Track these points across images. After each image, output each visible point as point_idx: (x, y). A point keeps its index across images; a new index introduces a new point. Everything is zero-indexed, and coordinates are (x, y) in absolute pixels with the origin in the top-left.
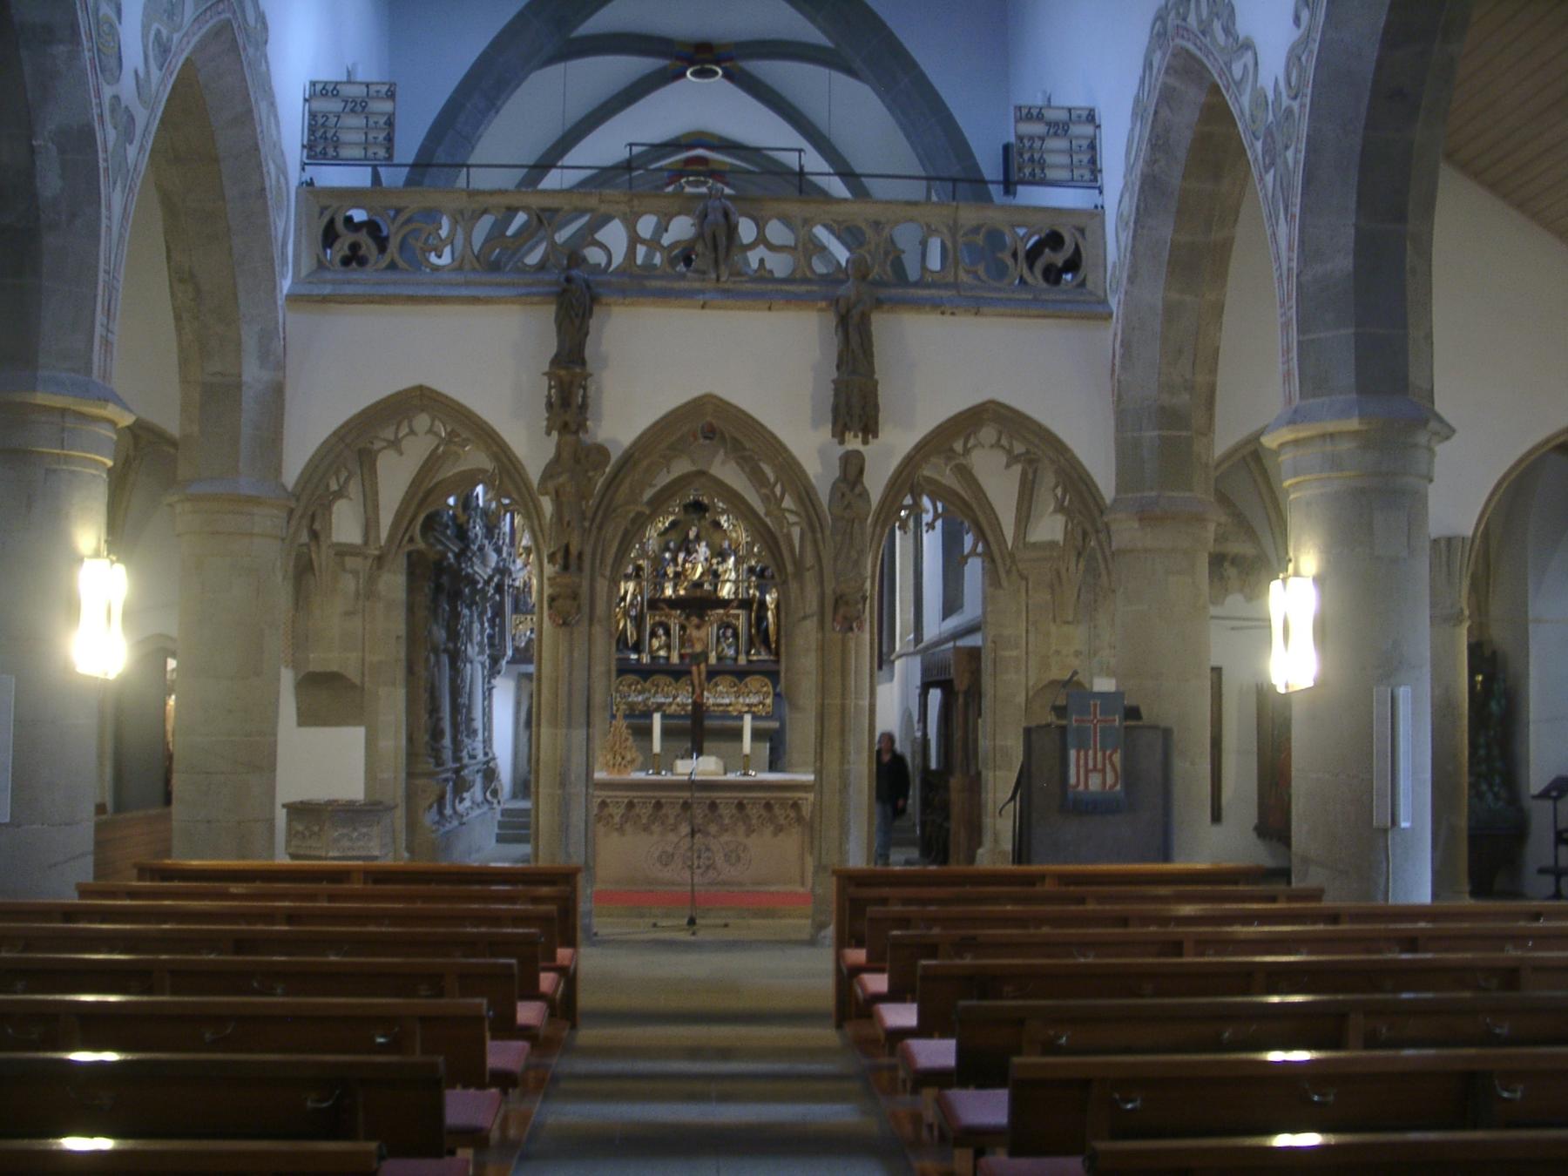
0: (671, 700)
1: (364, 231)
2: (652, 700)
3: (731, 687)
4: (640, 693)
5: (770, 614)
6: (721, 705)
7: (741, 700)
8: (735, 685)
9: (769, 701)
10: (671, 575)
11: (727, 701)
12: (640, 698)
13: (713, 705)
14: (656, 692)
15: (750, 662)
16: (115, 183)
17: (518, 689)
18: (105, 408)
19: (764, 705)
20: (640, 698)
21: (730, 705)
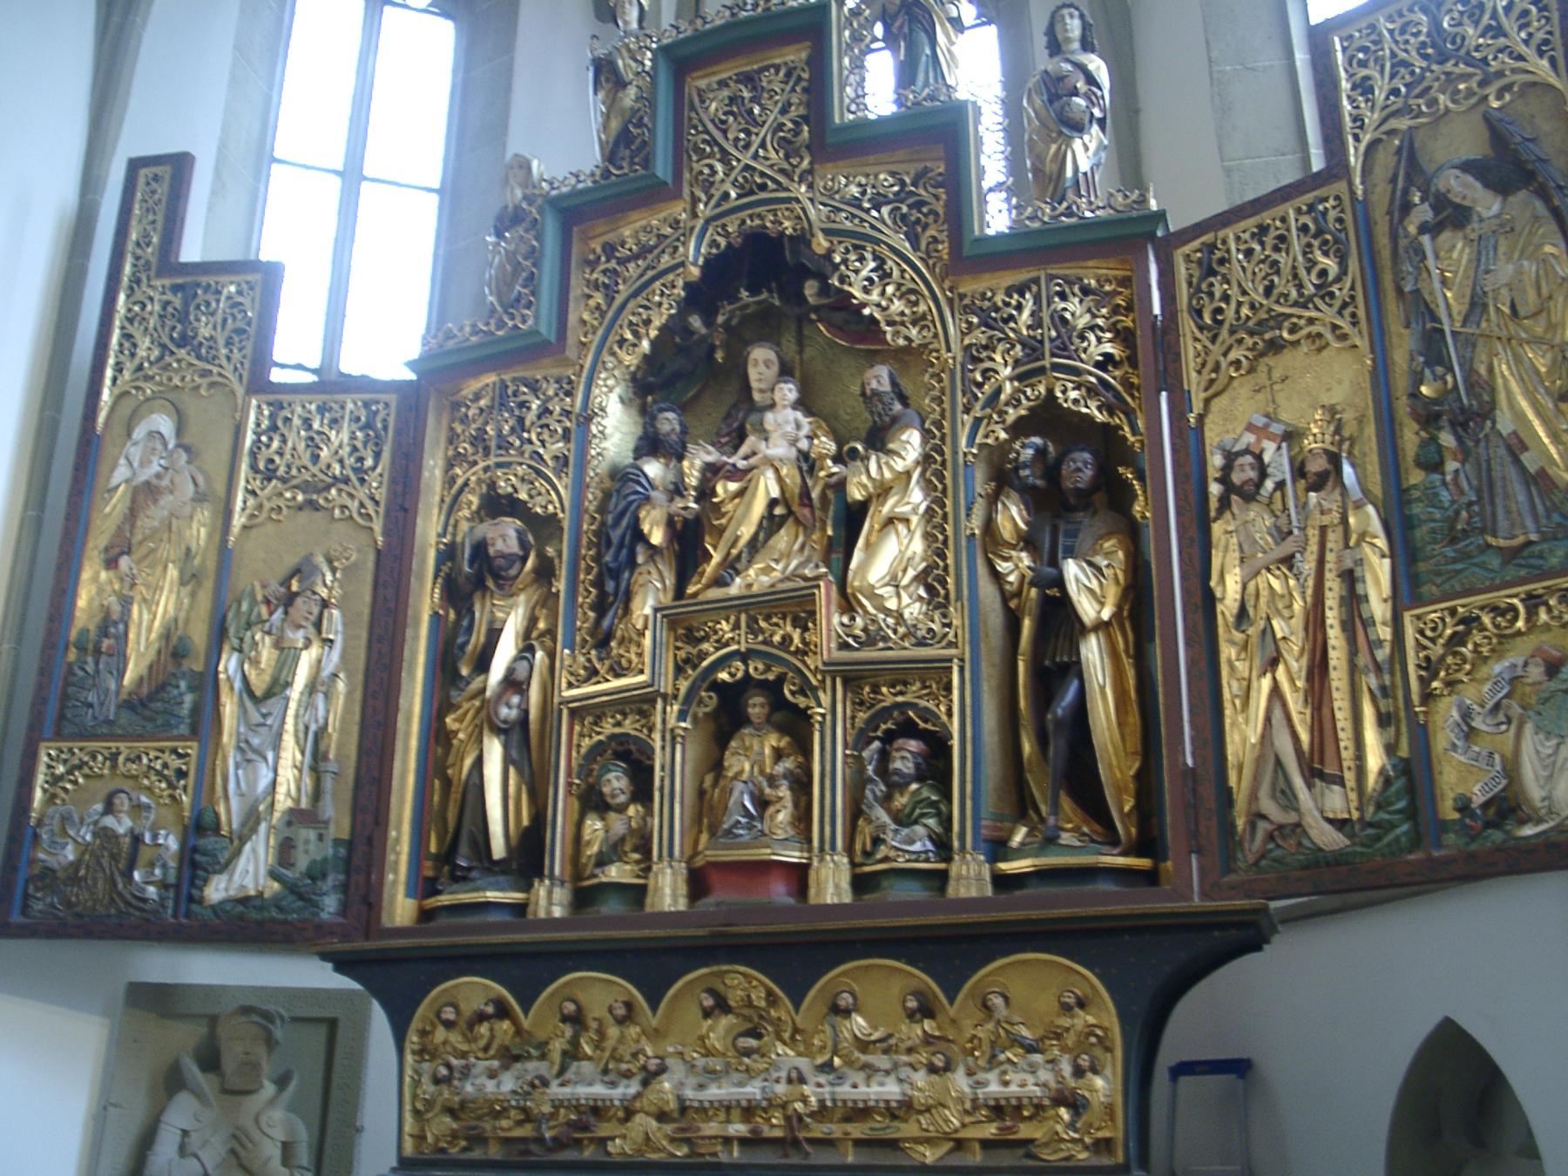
0: (633, 1088)
1: (816, 167)
2: (555, 1090)
3: (911, 1015)
4: (510, 1058)
5: (1092, 651)
6: (860, 1112)
7: (960, 1081)
8: (926, 1010)
9: (1102, 1086)
10: (657, 537)
11: (891, 1090)
12: (508, 1083)
13: (822, 1112)
14: (572, 1054)
15: (1002, 882)
16: (969, 509)
17: (121, 1049)
18: (408, 895)
19: (1077, 1105)
20: (508, 1083)
21: (904, 1109)
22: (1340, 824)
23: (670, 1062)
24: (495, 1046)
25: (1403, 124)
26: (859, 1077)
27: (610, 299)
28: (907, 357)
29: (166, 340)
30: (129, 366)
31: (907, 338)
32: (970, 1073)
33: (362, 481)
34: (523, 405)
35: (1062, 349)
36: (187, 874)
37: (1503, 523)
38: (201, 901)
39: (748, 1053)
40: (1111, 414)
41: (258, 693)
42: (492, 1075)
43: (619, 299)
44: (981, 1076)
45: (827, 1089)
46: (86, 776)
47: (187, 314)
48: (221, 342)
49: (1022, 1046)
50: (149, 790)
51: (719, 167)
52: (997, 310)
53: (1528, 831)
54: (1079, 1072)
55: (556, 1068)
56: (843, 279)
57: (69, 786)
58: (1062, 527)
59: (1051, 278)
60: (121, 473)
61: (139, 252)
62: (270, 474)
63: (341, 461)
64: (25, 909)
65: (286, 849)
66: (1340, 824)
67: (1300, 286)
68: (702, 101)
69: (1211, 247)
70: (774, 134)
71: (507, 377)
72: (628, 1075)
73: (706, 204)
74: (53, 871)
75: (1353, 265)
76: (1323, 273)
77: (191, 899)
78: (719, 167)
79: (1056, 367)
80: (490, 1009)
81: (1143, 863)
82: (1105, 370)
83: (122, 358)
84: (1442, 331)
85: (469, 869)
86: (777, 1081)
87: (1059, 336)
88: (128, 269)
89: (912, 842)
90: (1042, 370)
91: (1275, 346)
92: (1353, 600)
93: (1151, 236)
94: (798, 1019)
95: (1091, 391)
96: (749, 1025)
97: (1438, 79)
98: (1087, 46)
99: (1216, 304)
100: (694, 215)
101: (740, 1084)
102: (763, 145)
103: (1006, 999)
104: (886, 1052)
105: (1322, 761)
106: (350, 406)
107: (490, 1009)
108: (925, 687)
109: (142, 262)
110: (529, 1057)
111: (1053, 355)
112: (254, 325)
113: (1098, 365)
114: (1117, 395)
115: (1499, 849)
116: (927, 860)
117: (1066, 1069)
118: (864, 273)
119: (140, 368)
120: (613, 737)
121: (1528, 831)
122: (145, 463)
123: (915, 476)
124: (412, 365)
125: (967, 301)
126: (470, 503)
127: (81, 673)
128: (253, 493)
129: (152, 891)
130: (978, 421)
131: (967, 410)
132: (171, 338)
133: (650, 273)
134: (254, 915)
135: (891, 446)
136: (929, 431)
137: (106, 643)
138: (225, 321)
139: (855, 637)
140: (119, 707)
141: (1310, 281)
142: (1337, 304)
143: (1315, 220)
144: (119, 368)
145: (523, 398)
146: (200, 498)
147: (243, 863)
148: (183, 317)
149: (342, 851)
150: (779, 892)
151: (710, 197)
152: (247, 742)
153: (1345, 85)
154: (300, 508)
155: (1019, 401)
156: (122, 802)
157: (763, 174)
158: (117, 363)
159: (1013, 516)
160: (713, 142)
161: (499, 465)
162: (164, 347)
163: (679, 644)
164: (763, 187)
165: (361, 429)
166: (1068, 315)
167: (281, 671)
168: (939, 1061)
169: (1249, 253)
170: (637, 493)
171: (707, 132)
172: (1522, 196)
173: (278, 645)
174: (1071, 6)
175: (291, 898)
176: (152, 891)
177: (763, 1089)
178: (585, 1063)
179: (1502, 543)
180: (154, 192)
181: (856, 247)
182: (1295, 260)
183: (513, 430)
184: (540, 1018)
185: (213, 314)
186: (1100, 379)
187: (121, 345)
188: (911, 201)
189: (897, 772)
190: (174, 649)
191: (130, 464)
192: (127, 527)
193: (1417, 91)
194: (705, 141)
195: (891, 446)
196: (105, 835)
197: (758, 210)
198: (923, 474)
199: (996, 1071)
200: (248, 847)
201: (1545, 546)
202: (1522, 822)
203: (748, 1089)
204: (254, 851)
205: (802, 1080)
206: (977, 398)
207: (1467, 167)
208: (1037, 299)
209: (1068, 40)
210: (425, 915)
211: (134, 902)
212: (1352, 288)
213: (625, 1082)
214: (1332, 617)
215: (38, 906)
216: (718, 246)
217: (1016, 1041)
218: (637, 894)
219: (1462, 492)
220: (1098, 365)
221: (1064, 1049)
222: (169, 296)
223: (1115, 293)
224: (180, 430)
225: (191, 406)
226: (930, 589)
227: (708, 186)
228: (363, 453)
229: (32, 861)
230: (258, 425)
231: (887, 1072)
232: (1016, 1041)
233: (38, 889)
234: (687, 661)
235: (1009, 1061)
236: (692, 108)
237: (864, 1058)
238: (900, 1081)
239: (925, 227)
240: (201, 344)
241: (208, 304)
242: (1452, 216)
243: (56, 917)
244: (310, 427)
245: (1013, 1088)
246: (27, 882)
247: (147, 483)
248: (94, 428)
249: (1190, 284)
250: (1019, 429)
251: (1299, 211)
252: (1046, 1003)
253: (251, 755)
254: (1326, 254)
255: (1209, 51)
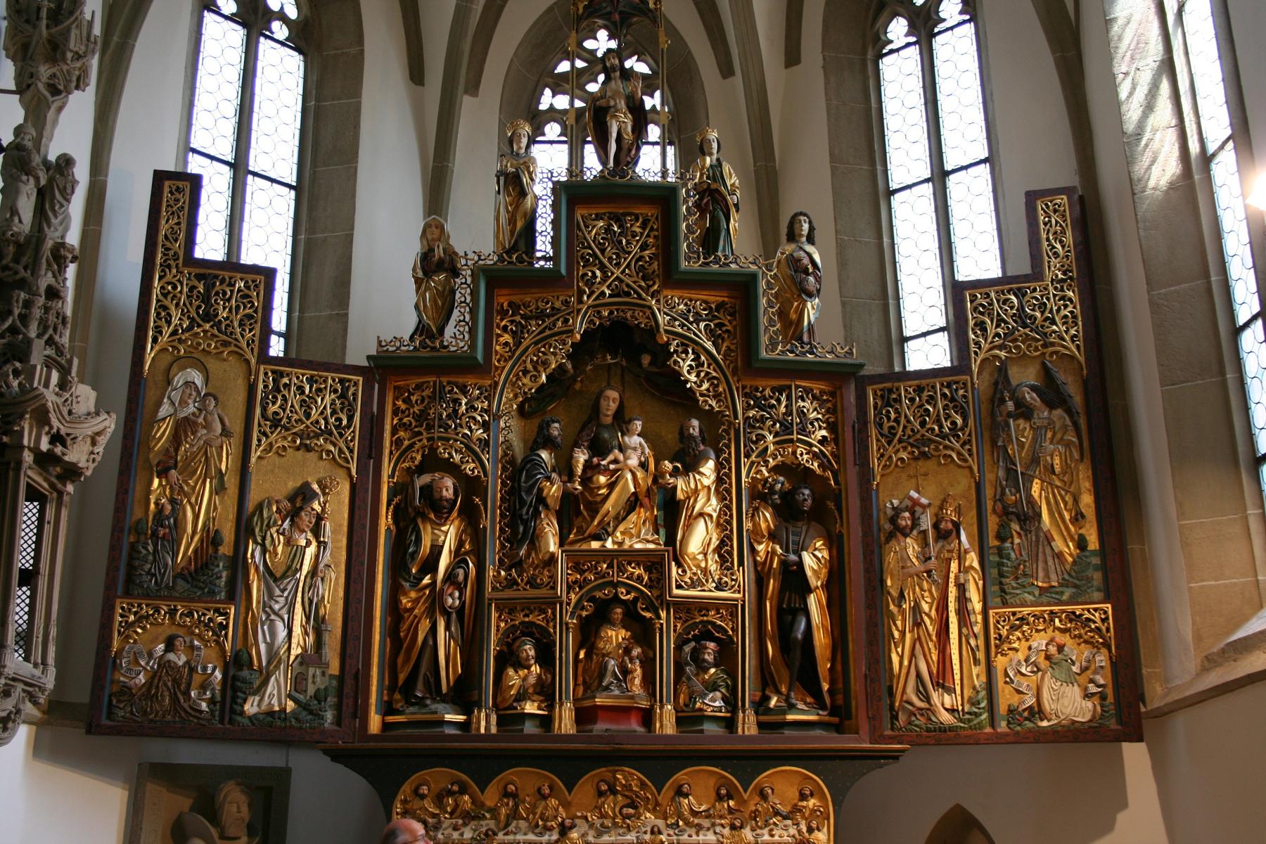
4: (468, 817)
18: (376, 713)
22: (952, 711)
23: (577, 821)
24: (459, 810)
25: (1003, 354)
26: (693, 831)
27: (518, 344)
28: (709, 418)
29: (193, 314)
30: (167, 331)
31: (710, 405)
32: (753, 830)
33: (341, 435)
34: (457, 402)
35: (803, 430)
36: (229, 693)
37: (1041, 574)
38: (242, 713)
39: (629, 817)
40: (824, 471)
41: (278, 575)
42: (455, 828)
43: (525, 344)
44: (759, 831)
45: (675, 837)
46: (151, 624)
47: (209, 298)
48: (236, 324)
49: (781, 815)
50: (200, 637)
51: (598, 273)
52: (765, 400)
53: (1045, 724)
54: (810, 830)
55: (502, 825)
56: (676, 362)
57: (139, 631)
58: (791, 529)
59: (797, 387)
60: (165, 410)
61: (168, 245)
62: (276, 423)
63: (325, 419)
64: (110, 714)
65: (299, 682)
66: (952, 711)
67: (941, 427)
68: (587, 227)
69: (890, 391)
70: (636, 262)
71: (445, 380)
72: (550, 829)
73: (589, 297)
74: (130, 689)
75: (971, 422)
76: (954, 423)
77: (233, 711)
78: (598, 273)
79: (799, 440)
80: (455, 788)
81: (836, 720)
82: (823, 445)
83: (159, 323)
84: (1017, 471)
85: (423, 698)
86: (645, 833)
87: (801, 422)
88: (159, 260)
89: (715, 701)
90: (791, 441)
91: (924, 455)
92: (963, 599)
93: (854, 374)
94: (659, 799)
95: (815, 456)
96: (629, 801)
97: (1021, 336)
98: (811, 240)
99: (892, 424)
100: (580, 301)
101: (623, 834)
102: (628, 266)
103: (773, 790)
104: (707, 817)
105: (944, 680)
106: (330, 381)
107: (455, 788)
108: (718, 613)
109: (172, 253)
110: (484, 818)
111: (798, 433)
112: (260, 311)
113: (819, 442)
114: (829, 461)
115: (1030, 730)
116: (721, 711)
117: (804, 828)
118: (689, 362)
119: (175, 333)
120: (522, 623)
121: (1045, 724)
122: (183, 403)
123: (713, 489)
124: (369, 358)
125: (747, 390)
126: (413, 459)
127: (144, 552)
128: (265, 434)
129: (204, 705)
130: (753, 463)
131: (747, 456)
132: (198, 313)
133: (548, 332)
134: (279, 723)
135: (701, 469)
136: (721, 464)
137: (162, 532)
138: (238, 307)
139: (686, 583)
140: (175, 577)
141: (947, 425)
142: (961, 442)
143: (951, 392)
144: (158, 330)
145: (456, 396)
146: (226, 433)
147: (271, 687)
148: (206, 298)
149: (334, 683)
150: (636, 726)
151: (592, 293)
152: (271, 607)
153: (971, 323)
154: (298, 449)
155: (776, 455)
156: (178, 642)
157: (628, 285)
158: (157, 327)
159: (766, 518)
160: (595, 256)
161: (440, 438)
162: (192, 320)
163: (569, 572)
164: (628, 294)
165: (339, 398)
166: (805, 410)
167: (293, 561)
168: (737, 823)
169: (912, 400)
170: (541, 473)
171: (590, 248)
172: (1058, 412)
173: (288, 542)
174: (805, 215)
175: (304, 713)
176: (204, 705)
177: (637, 837)
178: (521, 822)
179: (1040, 584)
180: (177, 200)
181: (683, 344)
182: (939, 411)
183: (449, 416)
184: (490, 796)
185: (229, 300)
186: (820, 450)
187: (158, 314)
188: (717, 321)
189: (705, 660)
190: (212, 539)
191: (173, 403)
192: (172, 450)
193: (1010, 338)
194: (588, 254)
195: (701, 469)
196: (164, 664)
197: (623, 307)
198: (716, 490)
199: (767, 829)
200: (273, 679)
201: (1061, 589)
202: (1042, 720)
203: (628, 837)
204: (277, 681)
205: (660, 833)
206: (753, 451)
207: (1033, 388)
208: (789, 398)
209: (802, 236)
210: (386, 726)
211: (193, 713)
212: (970, 435)
213: (548, 833)
214: (952, 606)
215: (121, 713)
216: (595, 324)
217: (777, 813)
218: (546, 722)
219: (1021, 555)
220: (819, 442)
221: (803, 817)
222: (196, 283)
223: (827, 401)
224: (207, 381)
225: (212, 364)
226: (720, 556)
227: (590, 283)
228: (341, 415)
229: (112, 682)
230: (266, 387)
231: (708, 829)
232: (777, 813)
233: (119, 701)
234: (575, 582)
235: (775, 823)
236: (580, 230)
237: (696, 821)
238: (715, 833)
239: (723, 340)
240: (220, 321)
241: (224, 293)
242: (1024, 411)
243: (135, 722)
244: (303, 393)
245: (777, 838)
246: (110, 696)
247: (186, 418)
248: (142, 373)
249: (875, 408)
250: (776, 470)
251: (942, 385)
252: (793, 794)
253: (273, 617)
254: (956, 412)
255: (836, 225)
